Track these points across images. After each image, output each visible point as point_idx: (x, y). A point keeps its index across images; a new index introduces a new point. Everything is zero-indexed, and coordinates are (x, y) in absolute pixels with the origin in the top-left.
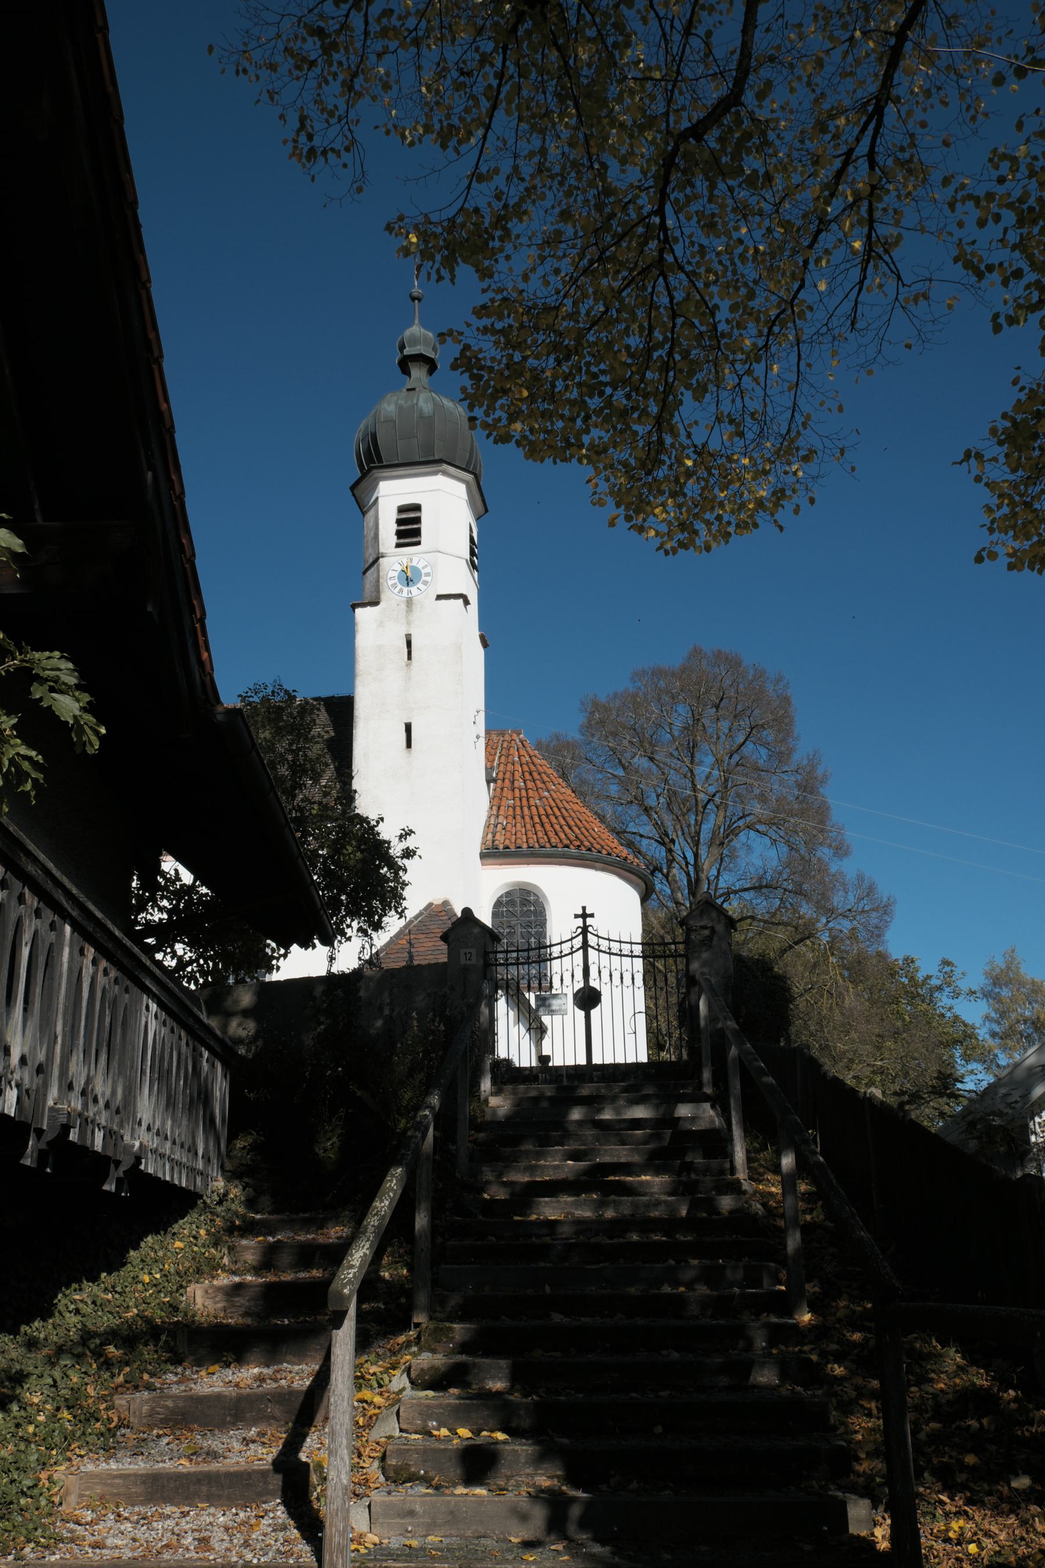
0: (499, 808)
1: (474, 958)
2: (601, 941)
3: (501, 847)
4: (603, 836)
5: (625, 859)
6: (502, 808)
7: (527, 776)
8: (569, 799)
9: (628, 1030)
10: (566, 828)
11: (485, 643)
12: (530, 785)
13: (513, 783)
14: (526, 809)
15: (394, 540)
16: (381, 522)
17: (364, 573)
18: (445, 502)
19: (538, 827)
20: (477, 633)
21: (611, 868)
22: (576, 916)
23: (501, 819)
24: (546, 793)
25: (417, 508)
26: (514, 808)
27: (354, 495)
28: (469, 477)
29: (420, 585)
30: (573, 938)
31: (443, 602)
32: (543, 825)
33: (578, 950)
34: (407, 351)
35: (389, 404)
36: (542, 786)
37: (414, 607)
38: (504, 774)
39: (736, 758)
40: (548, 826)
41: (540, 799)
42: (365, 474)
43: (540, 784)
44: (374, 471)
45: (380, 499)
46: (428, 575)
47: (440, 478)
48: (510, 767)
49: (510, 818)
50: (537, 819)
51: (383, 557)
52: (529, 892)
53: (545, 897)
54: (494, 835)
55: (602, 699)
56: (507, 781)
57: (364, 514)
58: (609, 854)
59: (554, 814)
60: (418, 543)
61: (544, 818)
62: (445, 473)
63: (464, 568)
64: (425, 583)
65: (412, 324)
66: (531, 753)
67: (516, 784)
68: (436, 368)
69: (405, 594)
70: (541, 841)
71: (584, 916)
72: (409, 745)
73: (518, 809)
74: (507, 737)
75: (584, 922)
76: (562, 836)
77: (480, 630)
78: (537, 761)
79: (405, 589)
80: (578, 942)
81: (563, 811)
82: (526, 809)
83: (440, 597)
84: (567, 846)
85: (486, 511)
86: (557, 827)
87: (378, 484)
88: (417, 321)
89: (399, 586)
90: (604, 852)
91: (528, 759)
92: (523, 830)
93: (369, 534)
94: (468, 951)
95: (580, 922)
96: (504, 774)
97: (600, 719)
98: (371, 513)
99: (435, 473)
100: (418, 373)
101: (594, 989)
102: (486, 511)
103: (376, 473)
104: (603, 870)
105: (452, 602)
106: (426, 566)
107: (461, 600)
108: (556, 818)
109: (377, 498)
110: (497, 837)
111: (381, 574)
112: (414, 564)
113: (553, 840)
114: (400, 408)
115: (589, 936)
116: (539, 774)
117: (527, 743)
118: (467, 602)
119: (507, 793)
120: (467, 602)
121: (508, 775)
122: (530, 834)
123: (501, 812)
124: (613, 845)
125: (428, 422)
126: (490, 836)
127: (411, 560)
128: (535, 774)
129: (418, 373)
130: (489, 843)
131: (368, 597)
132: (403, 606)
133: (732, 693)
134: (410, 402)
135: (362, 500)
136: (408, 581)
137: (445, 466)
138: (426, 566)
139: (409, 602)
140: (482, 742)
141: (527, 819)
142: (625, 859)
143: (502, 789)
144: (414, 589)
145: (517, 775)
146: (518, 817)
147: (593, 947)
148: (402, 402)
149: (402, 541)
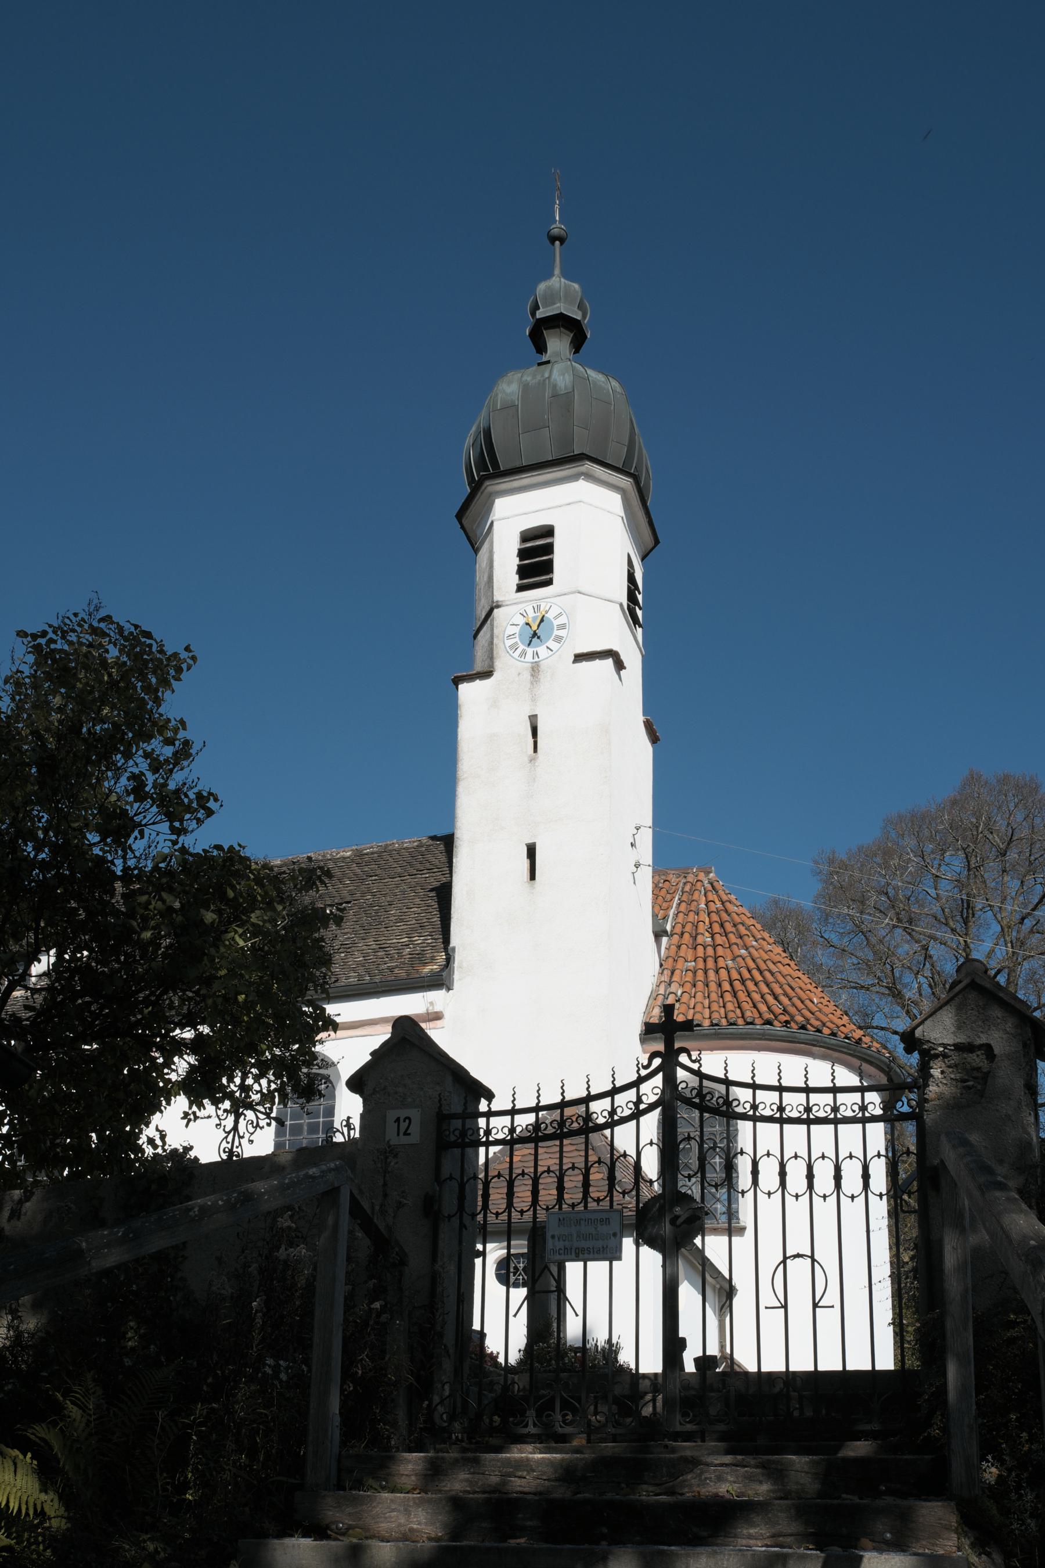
0: (672, 973)
1: (415, 1128)
4: (825, 1009)
6: (677, 972)
7: (717, 928)
8: (777, 958)
9: (767, 1298)
10: (770, 999)
11: (654, 737)
12: (719, 939)
13: (695, 938)
14: (712, 975)
15: (515, 580)
16: (496, 557)
17: (475, 636)
18: (589, 520)
19: (728, 997)
20: (641, 718)
23: (674, 987)
24: (743, 952)
25: (548, 531)
26: (695, 973)
27: (463, 527)
28: (626, 482)
29: (551, 643)
30: (641, 1080)
32: (735, 994)
33: (651, 1107)
34: (539, 315)
35: (510, 383)
36: (739, 941)
37: (541, 676)
38: (683, 927)
39: (1028, 923)
40: (742, 996)
41: (733, 960)
42: (476, 486)
43: (733, 938)
44: (487, 483)
45: (495, 524)
46: (562, 627)
48: (692, 917)
49: (688, 986)
50: (726, 986)
51: (498, 606)
55: (842, 855)
56: (686, 936)
57: (476, 551)
58: (834, 1034)
59: (753, 979)
60: (549, 582)
61: (737, 984)
62: (590, 477)
63: (618, 621)
64: (559, 639)
65: (550, 275)
66: (725, 898)
67: (700, 939)
68: (584, 337)
69: (529, 657)
70: (731, 1015)
72: (533, 876)
73: (700, 973)
74: (691, 878)
76: (763, 1008)
77: (644, 715)
78: (731, 908)
81: (767, 974)
82: (712, 975)
83: (579, 658)
84: (769, 1022)
85: (657, 542)
86: (756, 997)
88: (557, 271)
90: (826, 1031)
91: (719, 905)
92: (706, 1002)
93: (481, 578)
94: (402, 1113)
96: (683, 927)
97: (842, 887)
98: (486, 546)
99: (575, 478)
100: (558, 344)
102: (657, 542)
103: (491, 486)
105: (597, 662)
106: (560, 614)
107: (610, 662)
108: (756, 984)
109: (492, 523)
111: (496, 631)
113: (748, 1014)
114: (526, 388)
116: (735, 925)
117: (719, 885)
118: (619, 665)
119: (686, 952)
120: (619, 665)
121: (689, 928)
122: (715, 1006)
124: (840, 1022)
125: (564, 401)
128: (729, 927)
129: (558, 344)
131: (479, 667)
132: (527, 675)
133: (1025, 833)
134: (539, 377)
135: (470, 524)
137: (588, 466)
138: (560, 614)
139: (535, 669)
140: (646, 875)
141: (713, 986)
143: (679, 947)
144: (542, 650)
145: (702, 928)
146: (700, 985)
148: (528, 378)
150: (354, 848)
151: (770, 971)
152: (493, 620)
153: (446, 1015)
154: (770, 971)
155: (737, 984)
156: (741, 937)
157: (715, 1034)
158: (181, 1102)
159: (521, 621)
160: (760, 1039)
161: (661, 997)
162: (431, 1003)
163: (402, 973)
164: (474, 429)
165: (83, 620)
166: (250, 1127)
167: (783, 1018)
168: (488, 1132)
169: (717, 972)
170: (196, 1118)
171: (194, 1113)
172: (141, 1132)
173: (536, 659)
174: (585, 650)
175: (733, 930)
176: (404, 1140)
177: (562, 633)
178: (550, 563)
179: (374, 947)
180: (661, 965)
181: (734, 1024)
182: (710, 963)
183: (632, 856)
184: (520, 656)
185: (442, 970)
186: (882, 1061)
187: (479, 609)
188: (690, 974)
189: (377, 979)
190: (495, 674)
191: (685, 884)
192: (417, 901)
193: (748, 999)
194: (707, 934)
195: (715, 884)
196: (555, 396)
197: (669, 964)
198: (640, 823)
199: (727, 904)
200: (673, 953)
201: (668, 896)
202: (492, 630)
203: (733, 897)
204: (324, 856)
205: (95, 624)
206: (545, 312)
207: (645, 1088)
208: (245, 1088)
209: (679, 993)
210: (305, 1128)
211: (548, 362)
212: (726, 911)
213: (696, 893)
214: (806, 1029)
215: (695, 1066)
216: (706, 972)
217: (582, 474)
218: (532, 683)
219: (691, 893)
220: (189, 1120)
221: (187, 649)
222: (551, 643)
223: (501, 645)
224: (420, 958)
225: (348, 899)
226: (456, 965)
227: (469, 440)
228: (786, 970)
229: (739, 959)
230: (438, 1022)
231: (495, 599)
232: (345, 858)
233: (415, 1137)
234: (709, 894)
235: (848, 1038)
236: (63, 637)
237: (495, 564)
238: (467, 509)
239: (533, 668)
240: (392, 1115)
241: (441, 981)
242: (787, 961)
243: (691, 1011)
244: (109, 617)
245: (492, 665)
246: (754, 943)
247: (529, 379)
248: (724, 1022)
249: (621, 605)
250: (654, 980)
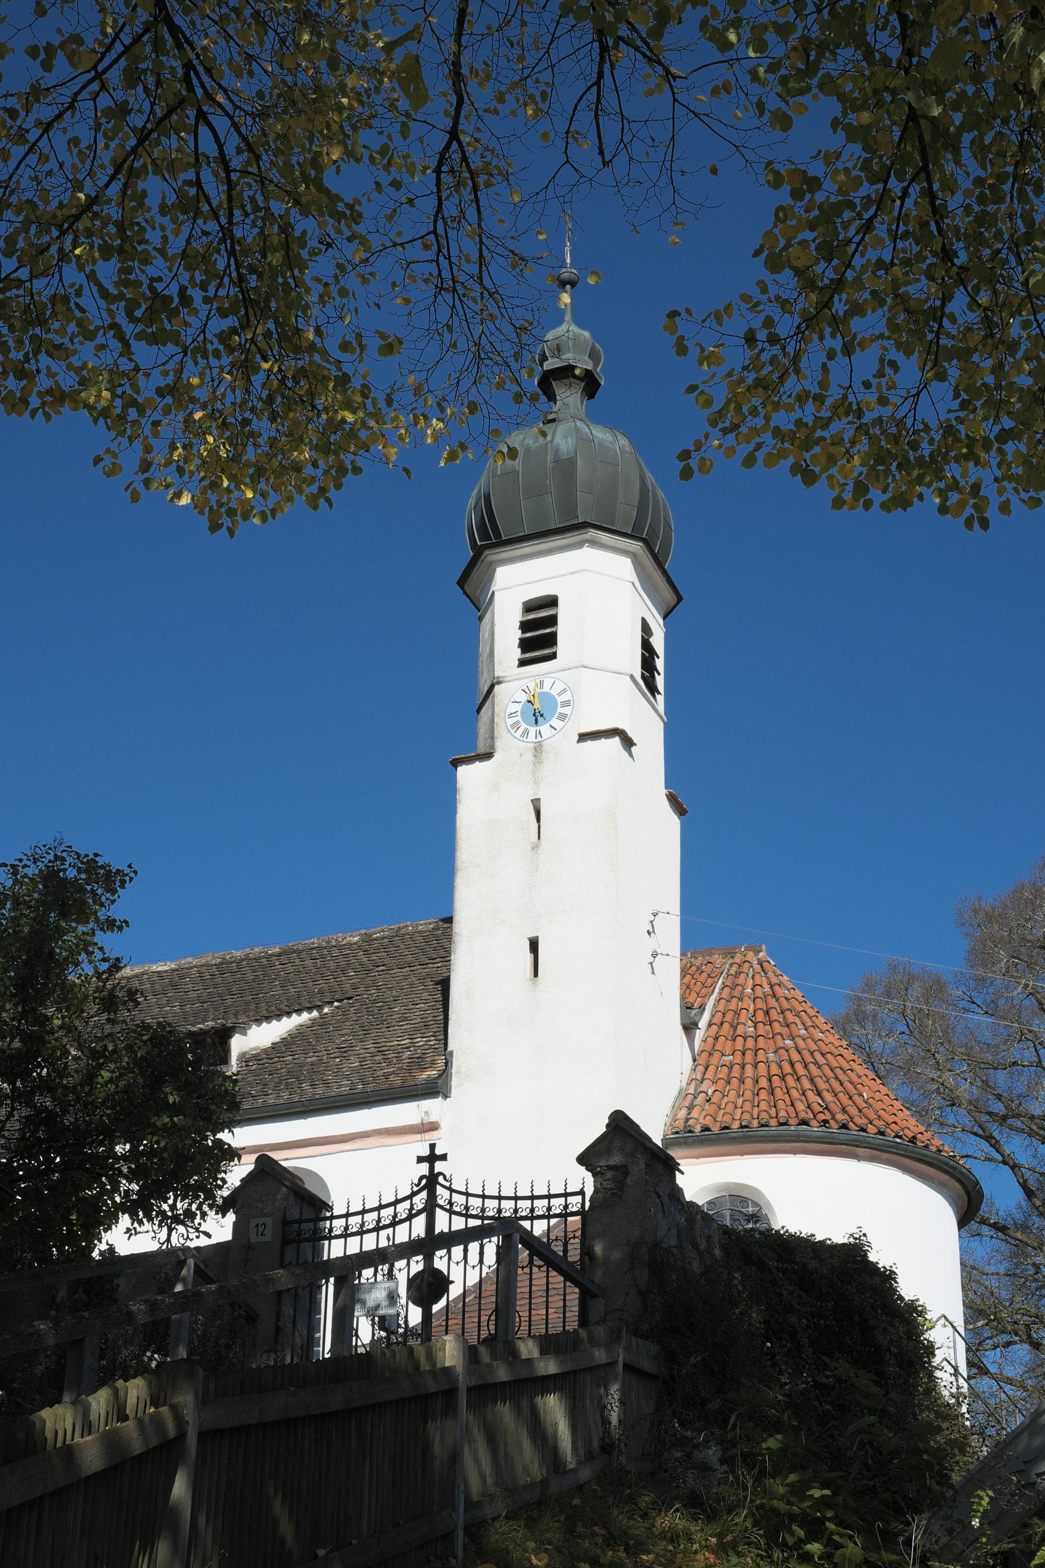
0: (706, 1069)
2: (456, 1197)
3: (698, 1129)
5: (913, 1140)
6: (712, 1068)
11: (680, 810)
12: (762, 1029)
15: (517, 653)
18: (601, 592)
20: (663, 792)
21: (885, 1155)
22: (420, 1160)
24: (788, 1042)
25: (552, 602)
26: (731, 1068)
27: (465, 593)
28: (636, 546)
29: (554, 722)
30: (414, 1194)
31: (589, 744)
34: (547, 366)
36: (785, 1031)
37: (544, 756)
41: (775, 1052)
42: (478, 552)
44: (487, 552)
46: (567, 703)
47: (587, 551)
50: (764, 1083)
51: (499, 683)
52: (744, 1201)
53: (770, 1206)
54: (690, 1108)
56: (726, 1026)
57: (481, 619)
58: (882, 1133)
60: (553, 656)
62: (594, 543)
64: (563, 717)
66: (774, 980)
67: (740, 1030)
73: (737, 1068)
74: (738, 959)
75: (432, 1168)
76: (801, 1106)
77: (666, 788)
79: (532, 730)
80: (420, 1200)
82: (749, 1070)
83: (583, 737)
84: (804, 1122)
85: (680, 598)
87: (494, 571)
89: (524, 726)
90: (871, 1129)
91: (767, 989)
94: (261, 1221)
95: (424, 1169)
99: (579, 545)
100: (569, 397)
101: (439, 1272)
102: (680, 598)
103: (490, 555)
104: (871, 1159)
105: (603, 741)
107: (616, 740)
109: (493, 593)
110: (695, 1114)
112: (546, 689)
115: (439, 1190)
118: (628, 743)
120: (628, 743)
121: (729, 1016)
123: (709, 1075)
125: (566, 467)
126: (683, 1113)
127: (542, 683)
128: (774, 1014)
129: (569, 397)
130: (680, 1124)
131: (481, 748)
132: (529, 756)
135: (472, 586)
136: (537, 717)
137: (592, 533)
139: (538, 749)
141: (749, 1082)
142: (913, 1140)
143: (716, 1039)
144: (545, 729)
146: (735, 1081)
147: (442, 1207)
149: (528, 655)
150: (363, 932)
152: (493, 698)
153: (443, 1125)
155: (776, 1080)
157: (744, 1137)
158: (125, 1221)
159: (524, 698)
160: (795, 1141)
161: (690, 1097)
162: (427, 1113)
163: (396, 1081)
164: (475, 492)
165: (50, 849)
166: (181, 1239)
168: (331, 1230)
169: (755, 1066)
170: (136, 1234)
171: (135, 1229)
172: (95, 1245)
173: (539, 739)
174: (589, 730)
176: (262, 1239)
178: (554, 635)
179: (372, 1050)
180: (694, 1060)
181: (766, 1126)
182: (749, 1056)
183: (650, 944)
184: (522, 735)
185: (440, 1076)
186: (941, 1161)
187: (482, 681)
188: (725, 1069)
189: (370, 1088)
190: (496, 755)
191: (731, 965)
192: (425, 996)
194: (750, 1023)
195: (765, 964)
196: (557, 461)
197: (702, 1060)
198: (657, 908)
199: (777, 988)
200: (708, 1047)
201: (710, 980)
202: (493, 707)
204: (328, 942)
205: (59, 854)
206: (552, 363)
207: (416, 1199)
208: (173, 1207)
209: (710, 1092)
211: (553, 420)
212: (774, 996)
213: (743, 976)
215: (447, 1184)
216: (743, 1067)
217: (587, 541)
219: (738, 974)
220: (131, 1235)
221: (130, 866)
222: (554, 722)
224: (420, 1063)
225: (349, 995)
226: (454, 1071)
227: (472, 502)
229: (782, 1052)
230: (434, 1133)
231: (496, 675)
232: (351, 944)
233: (268, 1237)
234: (757, 976)
235: (900, 1137)
236: (35, 862)
237: (496, 637)
238: (469, 576)
239: (535, 748)
240: (253, 1222)
241: (436, 1088)
243: (739, 1111)
244: (70, 847)
245: (492, 746)
246: (803, 1032)
247: (531, 442)
248: (773, 1122)
249: (632, 677)
250: (685, 1079)
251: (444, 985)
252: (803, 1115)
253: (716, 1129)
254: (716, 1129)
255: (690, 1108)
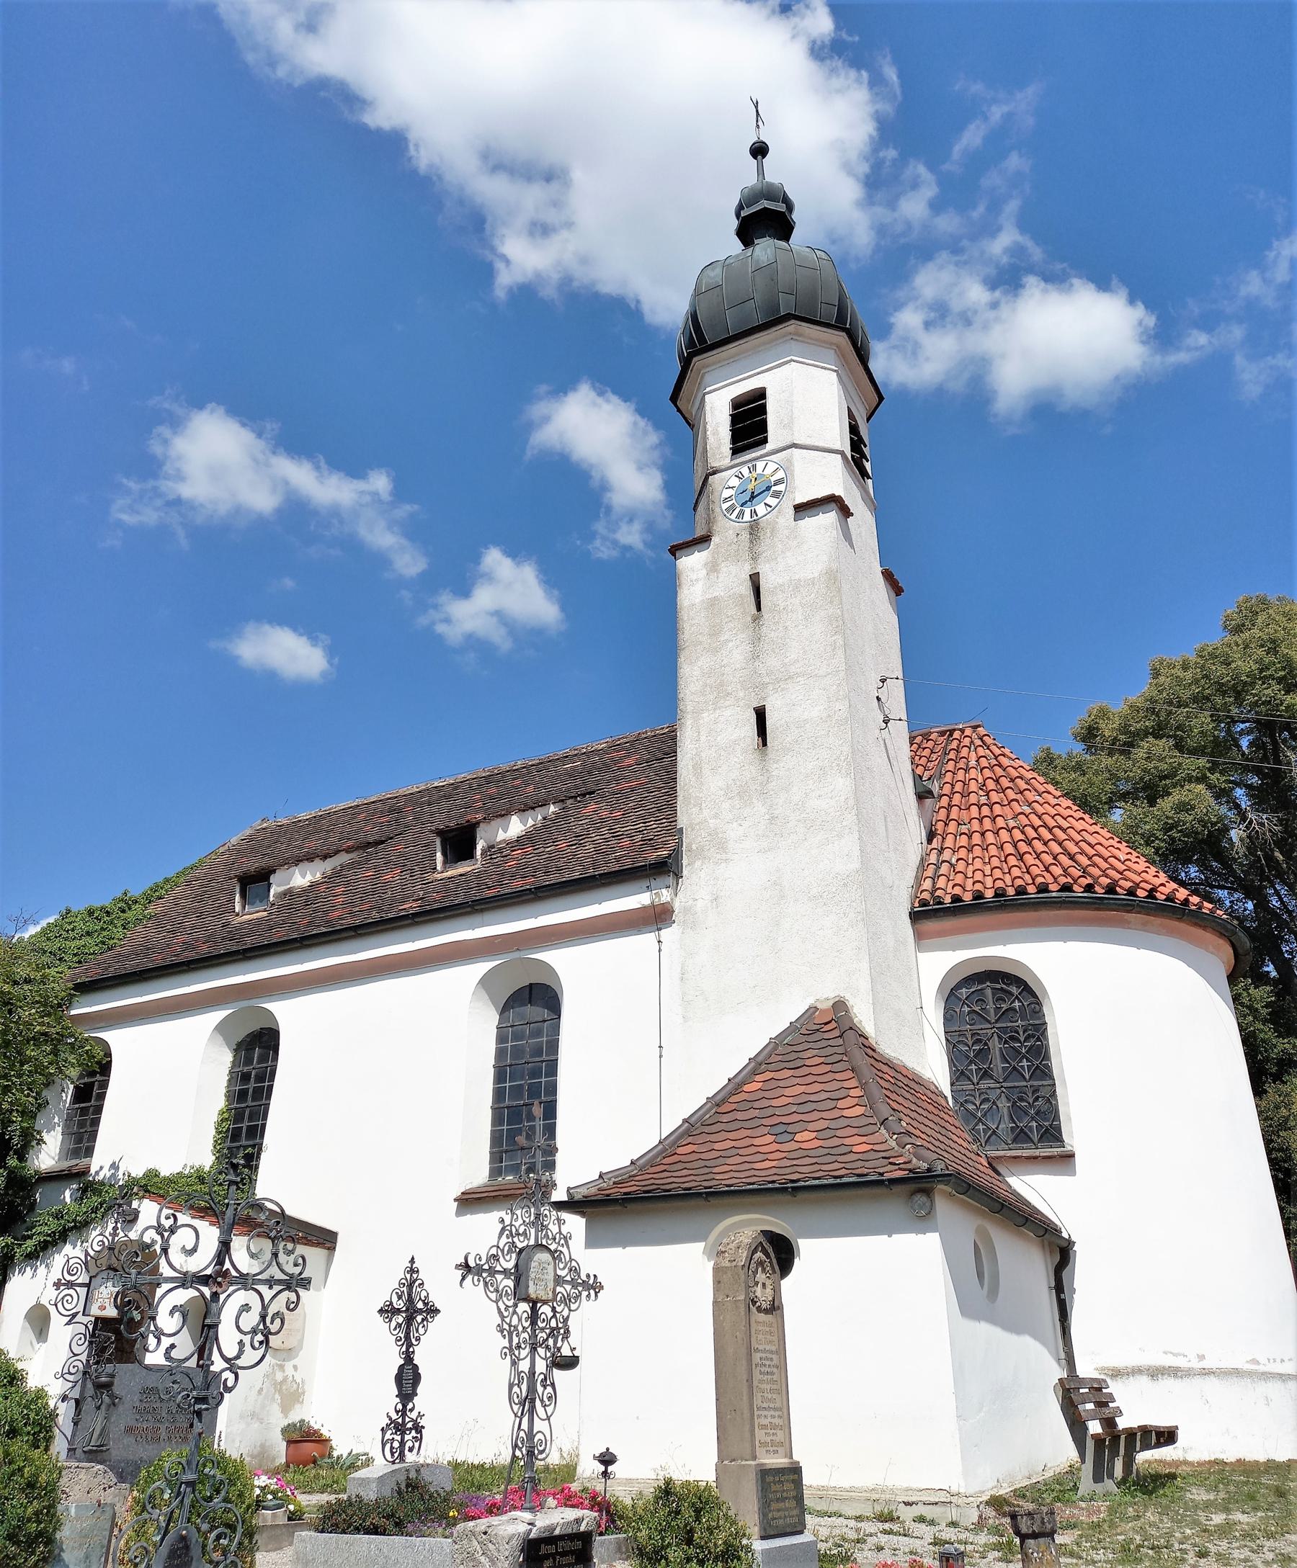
3: (948, 899)
4: (1135, 867)
12: (995, 797)
17: (695, 509)
20: (878, 569)
27: (679, 410)
28: (841, 338)
36: (1019, 797)
44: (695, 359)
51: (714, 473)
62: (796, 337)
66: (997, 752)
69: (747, 517)
71: (466, 1267)
78: (1005, 761)
102: (881, 398)
110: (941, 882)
116: (1012, 780)
120: (845, 512)
124: (1157, 882)
128: (1005, 782)
131: (699, 532)
132: (745, 536)
137: (792, 326)
145: (973, 786)
151: (1060, 827)
154: (1060, 827)
156: (1021, 793)
167: (1084, 882)
175: (1011, 785)
177: (781, 488)
178: (764, 406)
190: (715, 540)
193: (1037, 862)
203: (1007, 751)
209: (954, 861)
210: (1123, 1437)
212: (1000, 765)
214: (1116, 893)
218: (751, 542)
223: (718, 510)
228: (1080, 825)
239: (751, 527)
242: (1080, 814)
251: (1283, 1189)
252: (1063, 880)
253: (967, 897)
254: (967, 897)
255: (934, 879)
